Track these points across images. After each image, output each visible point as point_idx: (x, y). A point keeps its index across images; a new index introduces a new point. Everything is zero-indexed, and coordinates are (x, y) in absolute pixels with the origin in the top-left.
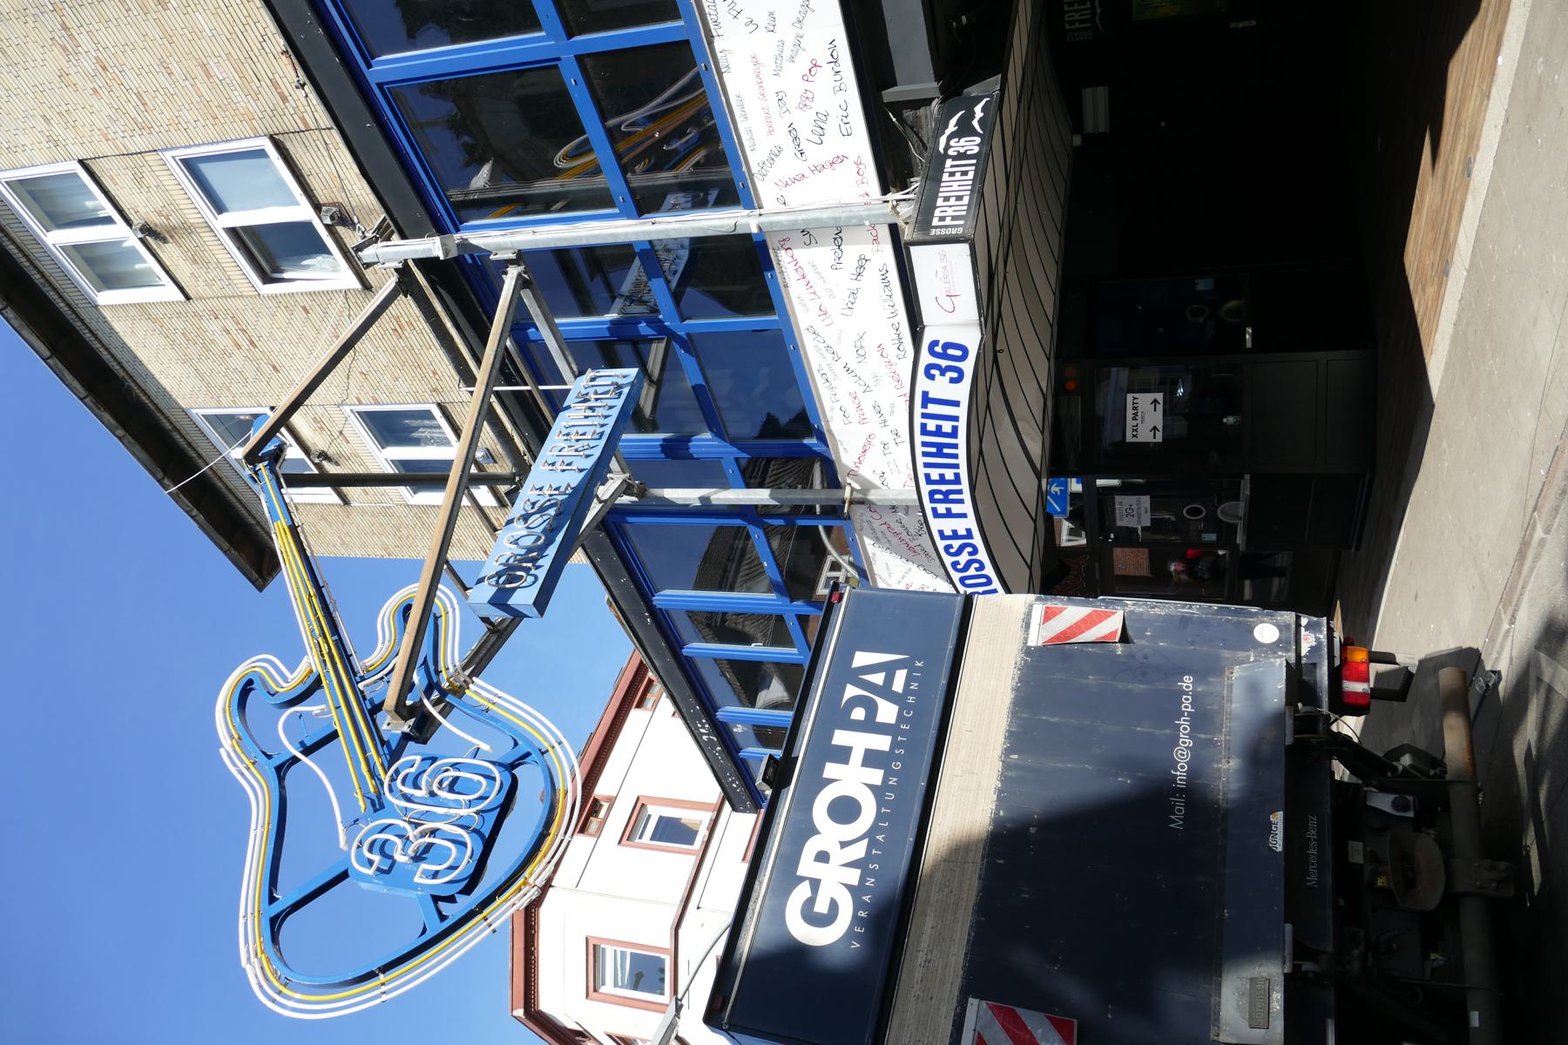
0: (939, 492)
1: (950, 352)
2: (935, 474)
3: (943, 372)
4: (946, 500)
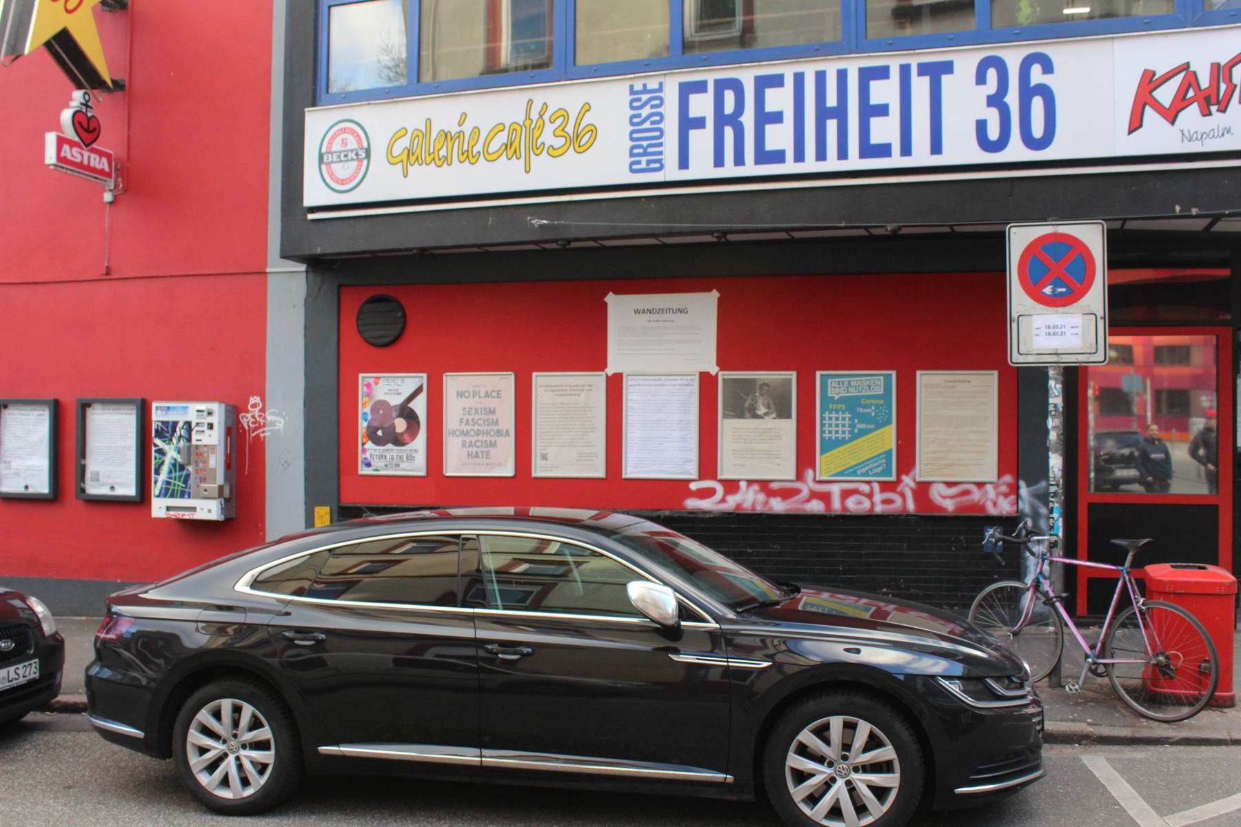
0: (640, 147)
1: (1037, 104)
2: (780, 99)
3: (996, 101)
4: (721, 120)
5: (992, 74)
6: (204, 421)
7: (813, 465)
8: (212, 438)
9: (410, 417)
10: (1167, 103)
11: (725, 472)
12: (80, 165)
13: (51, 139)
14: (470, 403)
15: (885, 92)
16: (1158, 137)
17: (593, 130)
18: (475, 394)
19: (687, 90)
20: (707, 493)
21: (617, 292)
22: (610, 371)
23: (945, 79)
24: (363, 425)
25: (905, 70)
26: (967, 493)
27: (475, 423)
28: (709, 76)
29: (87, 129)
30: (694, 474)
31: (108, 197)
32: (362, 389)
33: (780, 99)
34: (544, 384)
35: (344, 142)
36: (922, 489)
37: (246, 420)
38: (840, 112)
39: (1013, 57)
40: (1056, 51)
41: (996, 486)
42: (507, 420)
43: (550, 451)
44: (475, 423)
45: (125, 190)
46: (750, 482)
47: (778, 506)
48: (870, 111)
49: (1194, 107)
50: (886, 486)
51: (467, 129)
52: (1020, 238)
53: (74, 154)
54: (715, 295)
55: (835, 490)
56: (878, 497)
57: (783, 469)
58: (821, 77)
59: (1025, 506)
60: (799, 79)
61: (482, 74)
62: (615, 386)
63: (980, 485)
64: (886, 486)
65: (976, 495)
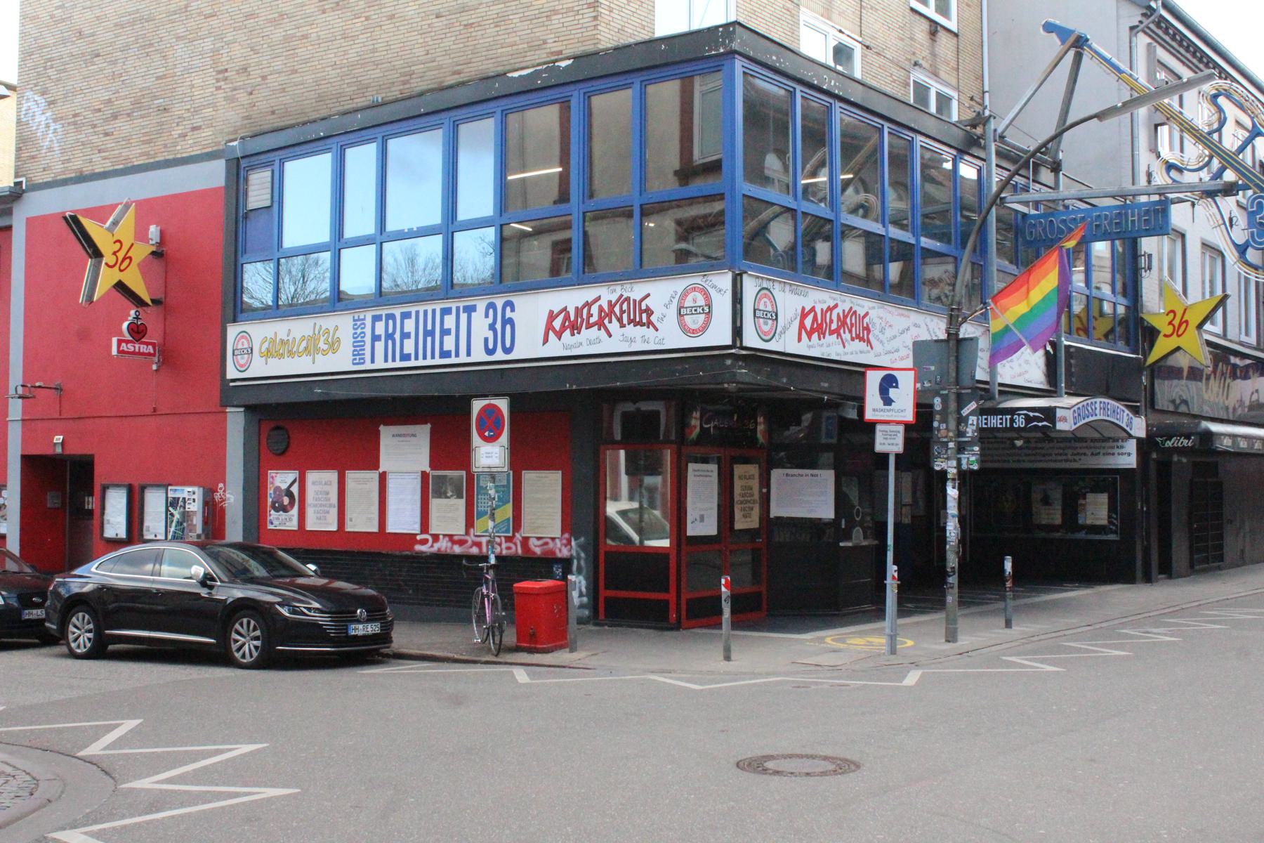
1: (508, 328)
3: (492, 327)
6: (193, 497)
7: (473, 526)
8: (195, 507)
9: (289, 494)
10: (557, 328)
11: (432, 531)
12: (134, 353)
13: (115, 340)
14: (318, 488)
15: (450, 322)
16: (555, 348)
17: (339, 340)
18: (320, 483)
19: (376, 318)
20: (424, 542)
21: (386, 424)
22: (381, 470)
24: (270, 500)
25: (458, 309)
26: (546, 544)
29: (138, 332)
30: (418, 531)
31: (154, 367)
32: (270, 480)
33: (409, 325)
34: (351, 476)
35: (695, 301)
36: (525, 540)
37: (217, 497)
38: (432, 333)
39: (499, 303)
40: (518, 300)
41: (561, 539)
42: (334, 500)
43: (354, 516)
44: (319, 499)
45: (163, 363)
46: (445, 536)
47: (457, 550)
49: (568, 331)
50: (509, 539)
51: (290, 338)
52: (477, 405)
53: (130, 347)
54: (429, 426)
55: (484, 540)
56: (504, 546)
57: (459, 529)
59: (574, 553)
60: (417, 312)
61: (555, 203)
62: (383, 478)
63: (553, 539)
64: (509, 539)
65: (551, 545)
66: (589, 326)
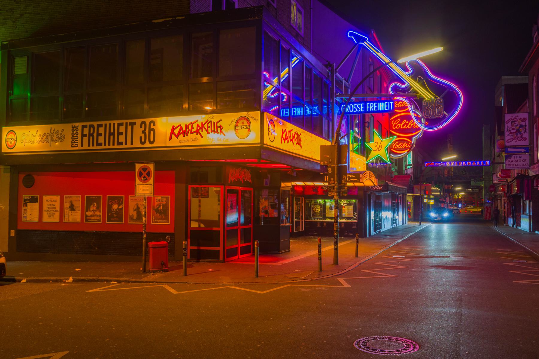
3: (144, 132)
5: (143, 125)
14: (49, 203)
15: (122, 129)
16: (176, 142)
17: (64, 136)
18: (51, 201)
19: (84, 127)
23: (134, 126)
25: (126, 123)
27: (50, 208)
28: (88, 124)
33: (101, 130)
38: (113, 134)
42: (58, 207)
44: (50, 208)
48: (120, 134)
49: (182, 135)
52: (138, 166)
58: (110, 125)
60: (106, 125)
66: (192, 133)
